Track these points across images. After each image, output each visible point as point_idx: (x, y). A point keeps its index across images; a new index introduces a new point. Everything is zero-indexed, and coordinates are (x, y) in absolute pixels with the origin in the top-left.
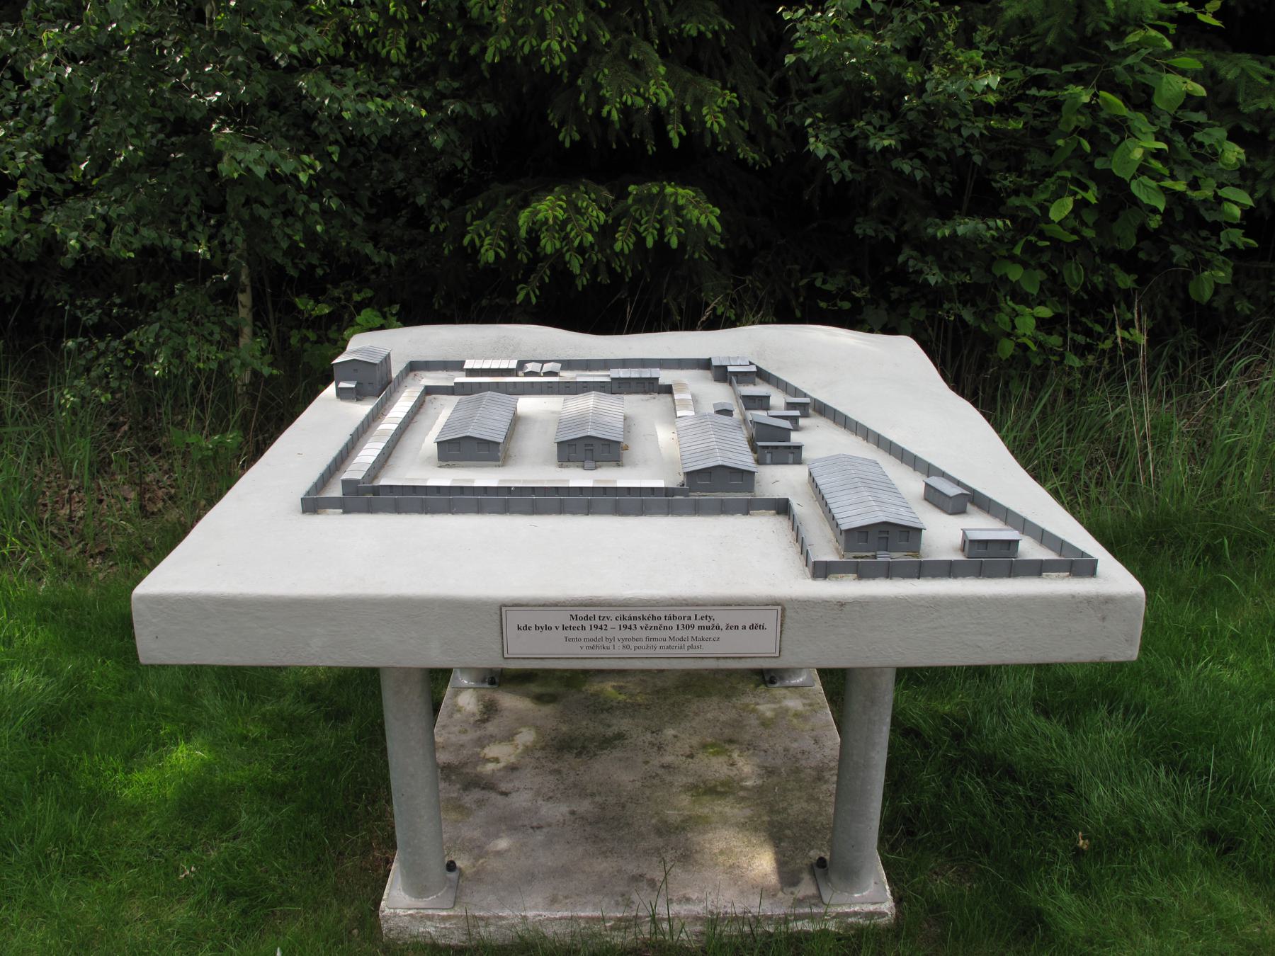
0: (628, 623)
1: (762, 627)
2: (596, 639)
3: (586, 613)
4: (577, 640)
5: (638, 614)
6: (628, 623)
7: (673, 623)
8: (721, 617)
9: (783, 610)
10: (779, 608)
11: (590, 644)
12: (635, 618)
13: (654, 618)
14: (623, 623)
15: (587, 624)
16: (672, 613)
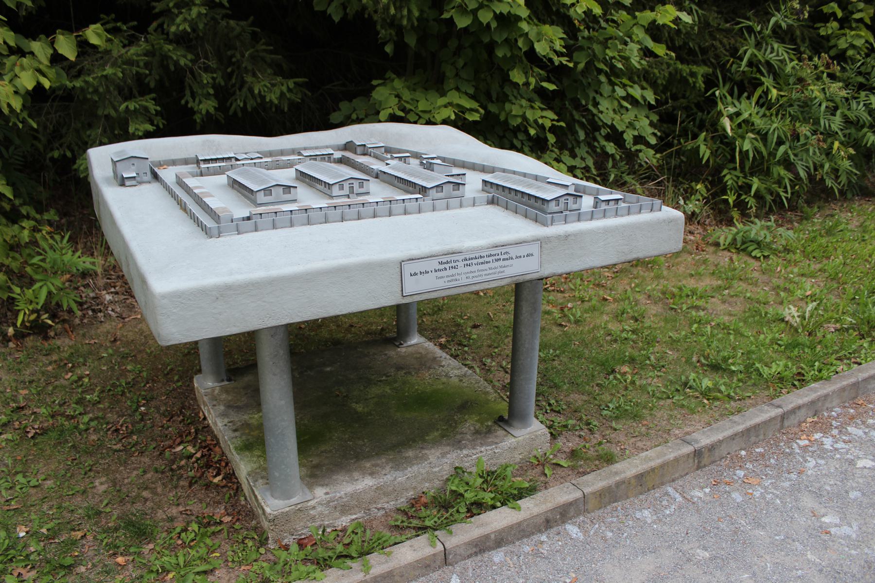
0: (468, 262)
1: (532, 255)
2: (453, 276)
3: (448, 259)
4: (442, 277)
5: (473, 256)
6: (468, 262)
7: (490, 259)
8: (514, 251)
11: (449, 279)
12: (472, 259)
13: (481, 257)
14: (466, 262)
15: (447, 266)
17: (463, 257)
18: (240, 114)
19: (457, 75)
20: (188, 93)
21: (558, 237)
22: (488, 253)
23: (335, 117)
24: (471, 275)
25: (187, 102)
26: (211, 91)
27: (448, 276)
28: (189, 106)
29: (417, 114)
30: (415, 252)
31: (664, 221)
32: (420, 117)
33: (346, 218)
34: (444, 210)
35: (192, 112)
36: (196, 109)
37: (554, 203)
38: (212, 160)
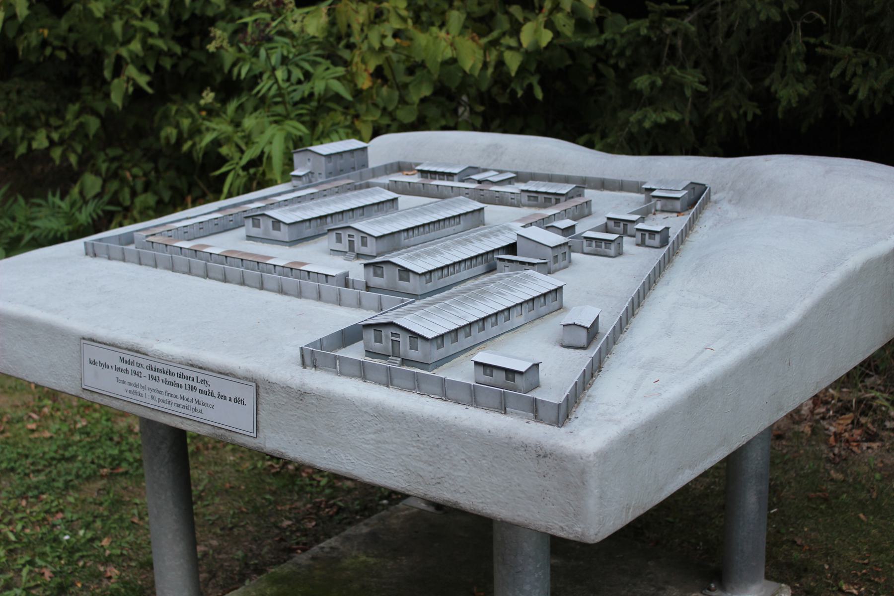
8: (216, 384)
9: (257, 386)
11: (132, 388)
14: (152, 373)
16: (182, 371)
23: (585, 138)
24: (158, 396)
26: (801, 67)
27: (130, 384)
31: (525, 447)
38: (443, 174)
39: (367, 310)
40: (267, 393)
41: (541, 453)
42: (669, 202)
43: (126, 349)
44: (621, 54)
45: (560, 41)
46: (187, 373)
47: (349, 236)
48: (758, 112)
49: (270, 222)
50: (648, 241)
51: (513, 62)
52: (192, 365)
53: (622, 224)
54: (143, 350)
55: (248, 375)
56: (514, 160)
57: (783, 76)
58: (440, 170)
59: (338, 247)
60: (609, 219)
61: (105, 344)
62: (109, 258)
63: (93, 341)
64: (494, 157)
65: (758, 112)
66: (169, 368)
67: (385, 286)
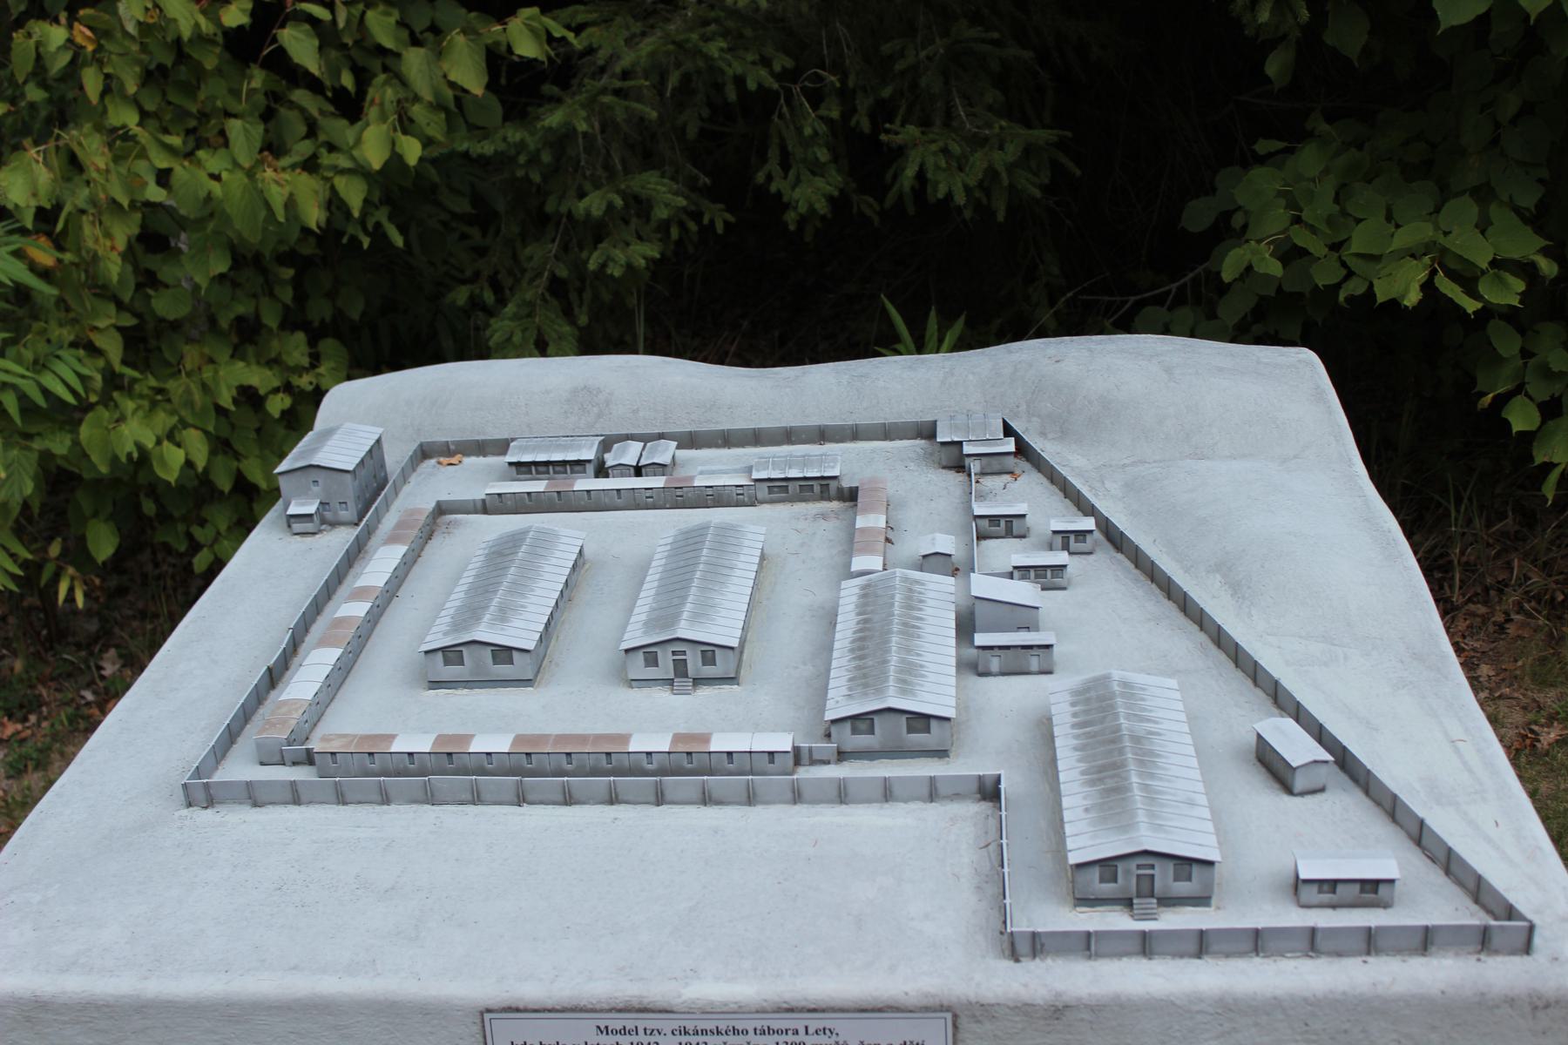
5: (710, 1025)
9: (955, 1017)
10: (949, 1016)
12: (704, 1032)
13: (735, 1031)
16: (766, 1024)
17: (675, 1025)
18: (911, 210)
19: (1495, 141)
20: (773, 153)
21: (1024, 1010)
22: (758, 1024)
25: (770, 178)
26: (823, 155)
28: (773, 188)
29: (1344, 264)
30: (531, 992)
31: (1511, 1001)
32: (1350, 274)
33: (529, 797)
34: (830, 801)
35: (779, 204)
36: (785, 199)
37: (1096, 872)
39: (906, 801)
40: (978, 1022)
41: (1539, 1003)
42: (994, 461)
43: (610, 1010)
44: (534, 160)
45: (435, 152)
46: (775, 1025)
47: (674, 653)
48: (730, 218)
49: (488, 652)
50: (1073, 545)
51: (354, 194)
52: (791, 1010)
53: (1003, 523)
54: (665, 1006)
55: (930, 1002)
56: (636, 411)
57: (785, 166)
58: (542, 457)
59: (652, 673)
60: (1055, 532)
61: (550, 1011)
62: (256, 805)
63: (518, 1010)
64: (596, 410)
65: (730, 218)
66: (731, 1023)
67: (877, 747)
